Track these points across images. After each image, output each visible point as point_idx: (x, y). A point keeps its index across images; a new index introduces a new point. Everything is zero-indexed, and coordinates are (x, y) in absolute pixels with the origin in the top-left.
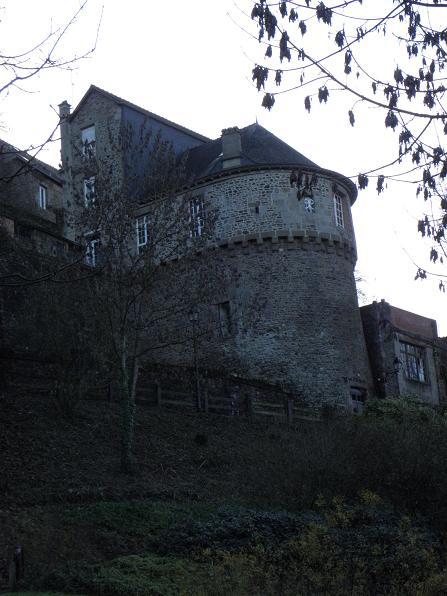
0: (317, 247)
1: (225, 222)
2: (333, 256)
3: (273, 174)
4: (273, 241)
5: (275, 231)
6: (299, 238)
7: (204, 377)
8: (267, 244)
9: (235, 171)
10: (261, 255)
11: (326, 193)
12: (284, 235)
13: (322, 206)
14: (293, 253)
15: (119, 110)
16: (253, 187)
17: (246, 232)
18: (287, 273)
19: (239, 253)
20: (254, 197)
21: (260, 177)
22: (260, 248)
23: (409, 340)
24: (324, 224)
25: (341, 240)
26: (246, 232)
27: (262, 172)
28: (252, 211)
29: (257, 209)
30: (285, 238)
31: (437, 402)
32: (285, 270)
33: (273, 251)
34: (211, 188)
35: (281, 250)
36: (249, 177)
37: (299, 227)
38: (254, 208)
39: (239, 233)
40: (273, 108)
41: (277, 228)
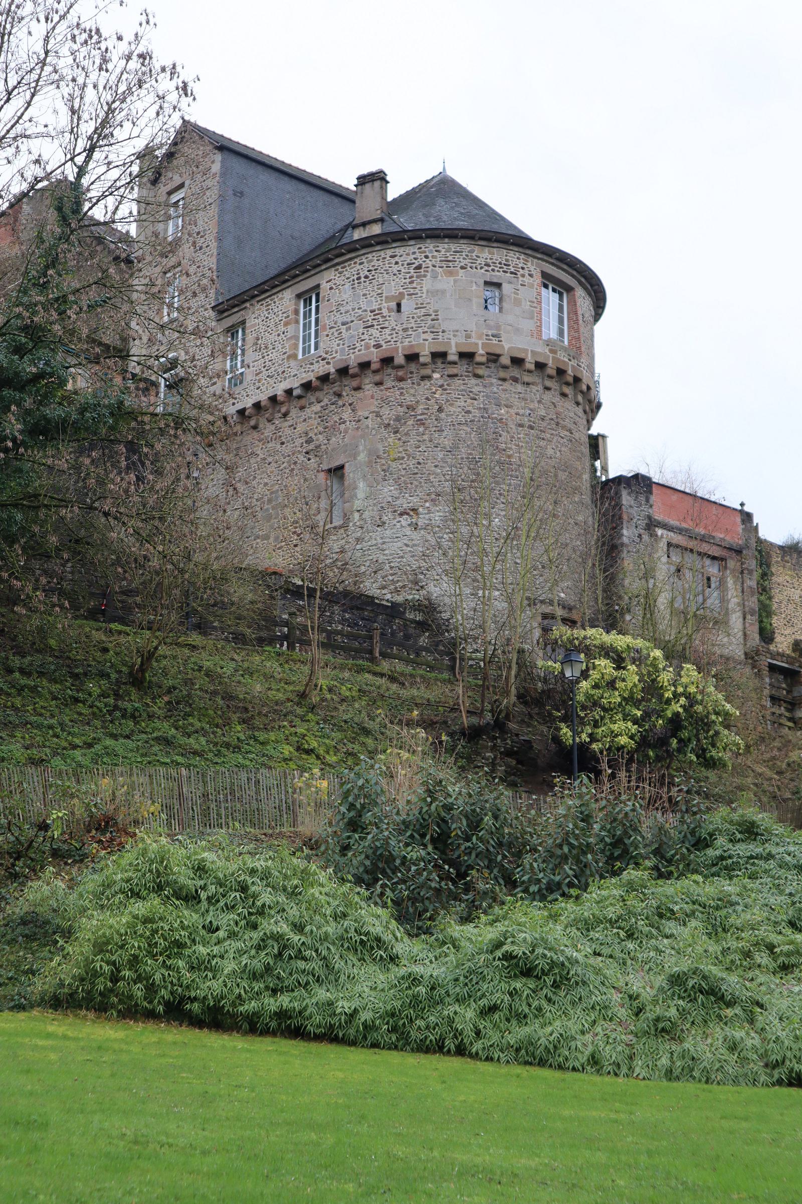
0: (502, 374)
1: (348, 329)
2: (534, 388)
3: (429, 246)
4: (422, 359)
5: (425, 347)
6: (467, 356)
7: (119, 473)
8: (413, 367)
9: (367, 244)
10: (401, 384)
11: (527, 279)
12: (442, 349)
13: (518, 302)
14: (457, 382)
15: (218, 157)
16: (395, 268)
17: (378, 346)
18: (443, 415)
19: (368, 382)
20: (393, 287)
21: (408, 253)
22: (400, 373)
23: (691, 544)
24: (517, 331)
25: (550, 363)
26: (378, 346)
27: (412, 242)
28: (390, 310)
29: (399, 305)
30: (443, 355)
31: (380, 225)
32: (440, 410)
33: (423, 378)
34: (331, 274)
35: (436, 376)
36: (389, 252)
37: (468, 337)
38: (393, 305)
39: (367, 347)
40: (606, 434)
41: (430, 337)
